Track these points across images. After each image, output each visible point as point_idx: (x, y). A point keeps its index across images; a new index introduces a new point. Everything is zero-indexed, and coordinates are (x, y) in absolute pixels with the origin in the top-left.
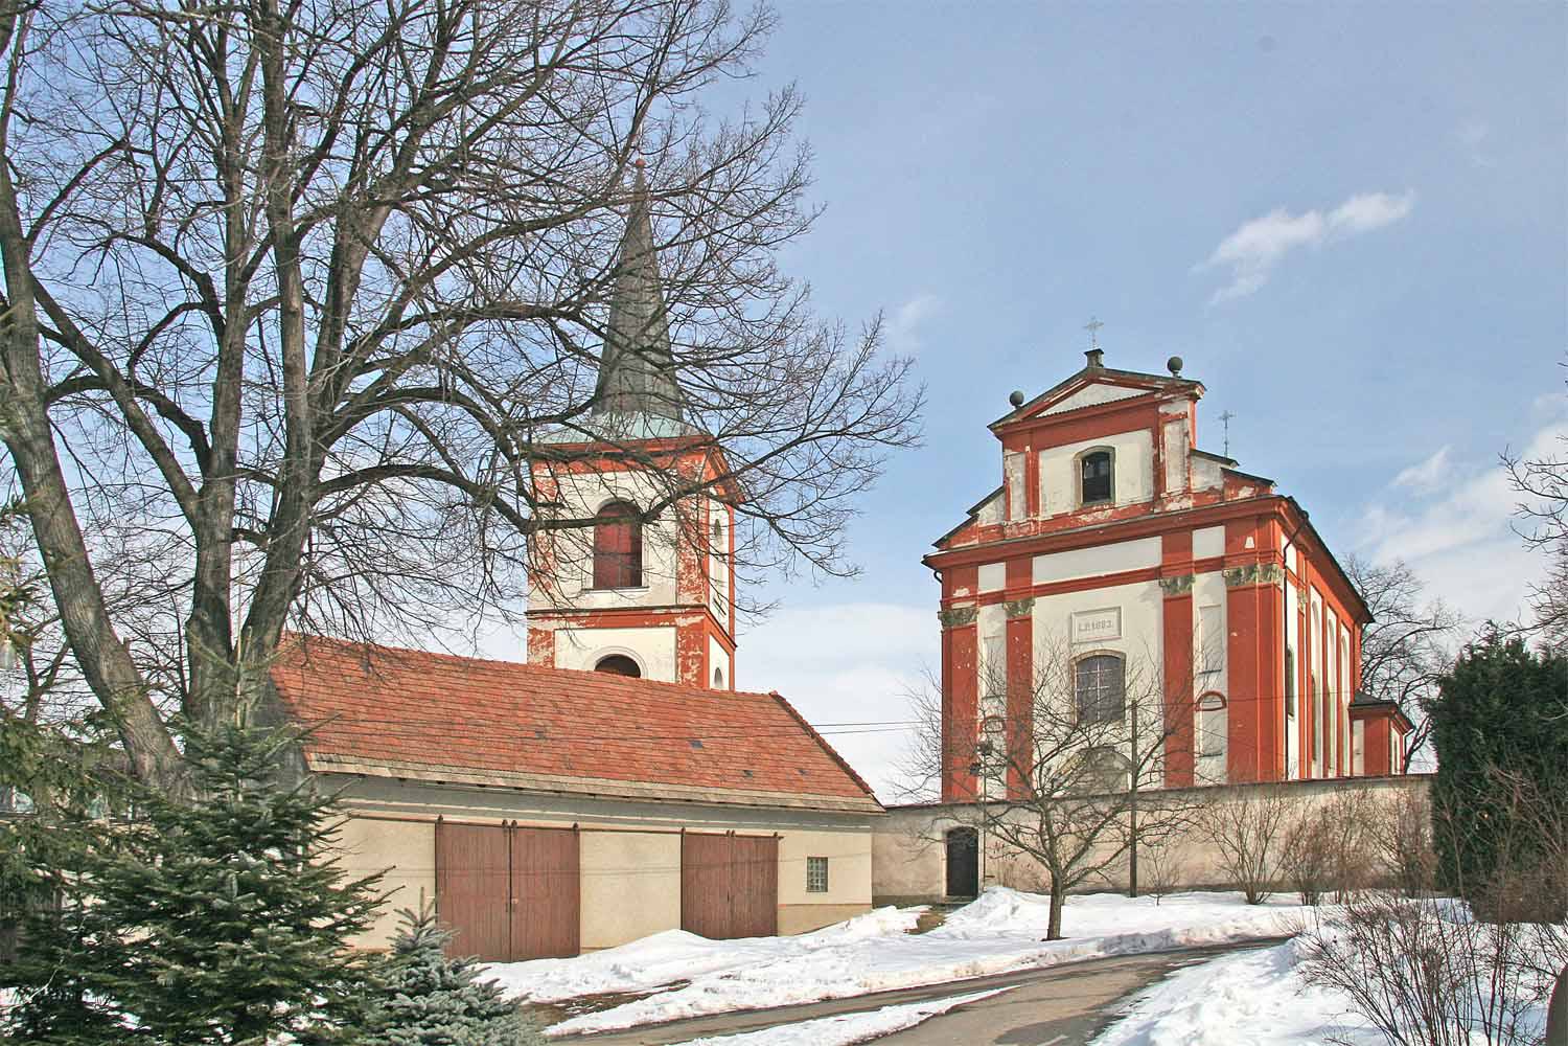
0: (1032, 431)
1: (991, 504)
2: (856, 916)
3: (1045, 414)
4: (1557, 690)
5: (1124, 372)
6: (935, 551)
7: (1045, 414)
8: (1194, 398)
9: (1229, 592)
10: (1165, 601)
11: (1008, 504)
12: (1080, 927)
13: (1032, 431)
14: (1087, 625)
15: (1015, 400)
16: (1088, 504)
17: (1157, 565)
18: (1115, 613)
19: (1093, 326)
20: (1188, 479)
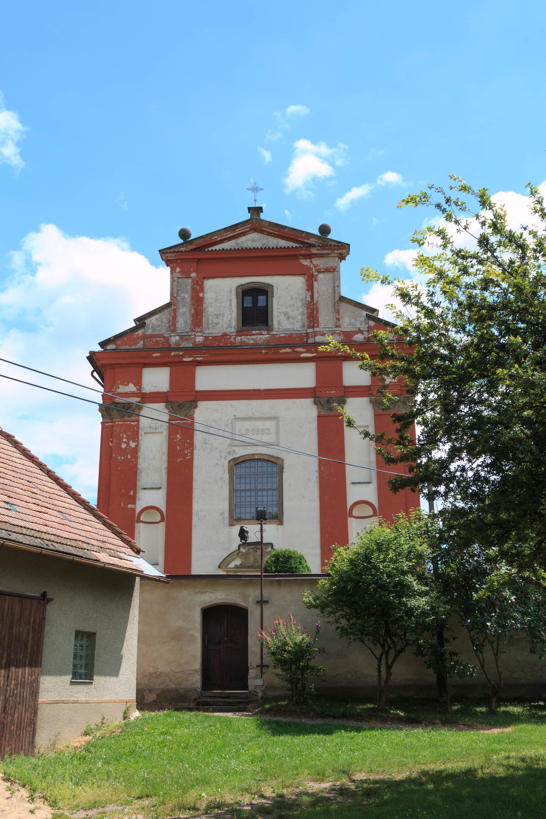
0: (199, 261)
1: (157, 316)
2: (61, 226)
3: (214, 248)
4: (506, 491)
5: (286, 227)
6: (98, 349)
7: (214, 248)
8: (342, 257)
9: (375, 415)
10: (319, 416)
11: (174, 318)
12: (285, 791)
13: (199, 261)
14: (247, 430)
15: (184, 234)
16: (245, 328)
17: (166, 391)
18: (273, 423)
19: (255, 189)
20: (338, 319)
